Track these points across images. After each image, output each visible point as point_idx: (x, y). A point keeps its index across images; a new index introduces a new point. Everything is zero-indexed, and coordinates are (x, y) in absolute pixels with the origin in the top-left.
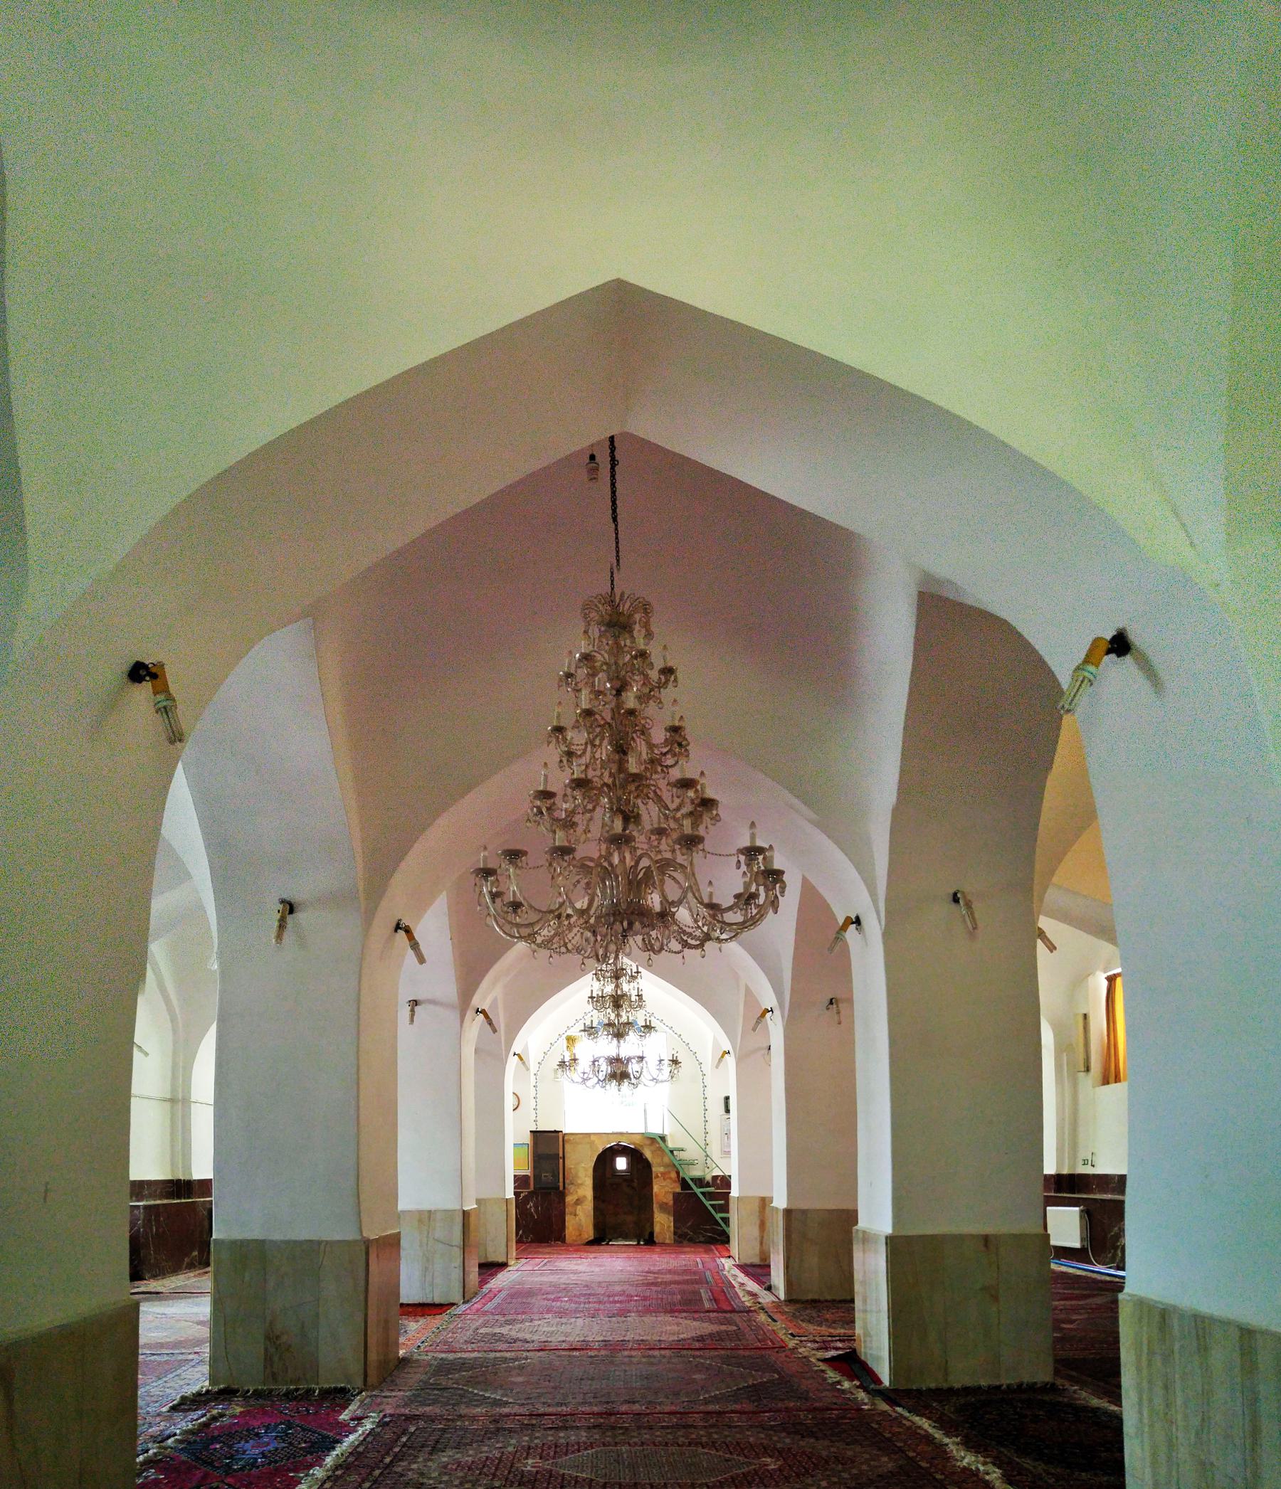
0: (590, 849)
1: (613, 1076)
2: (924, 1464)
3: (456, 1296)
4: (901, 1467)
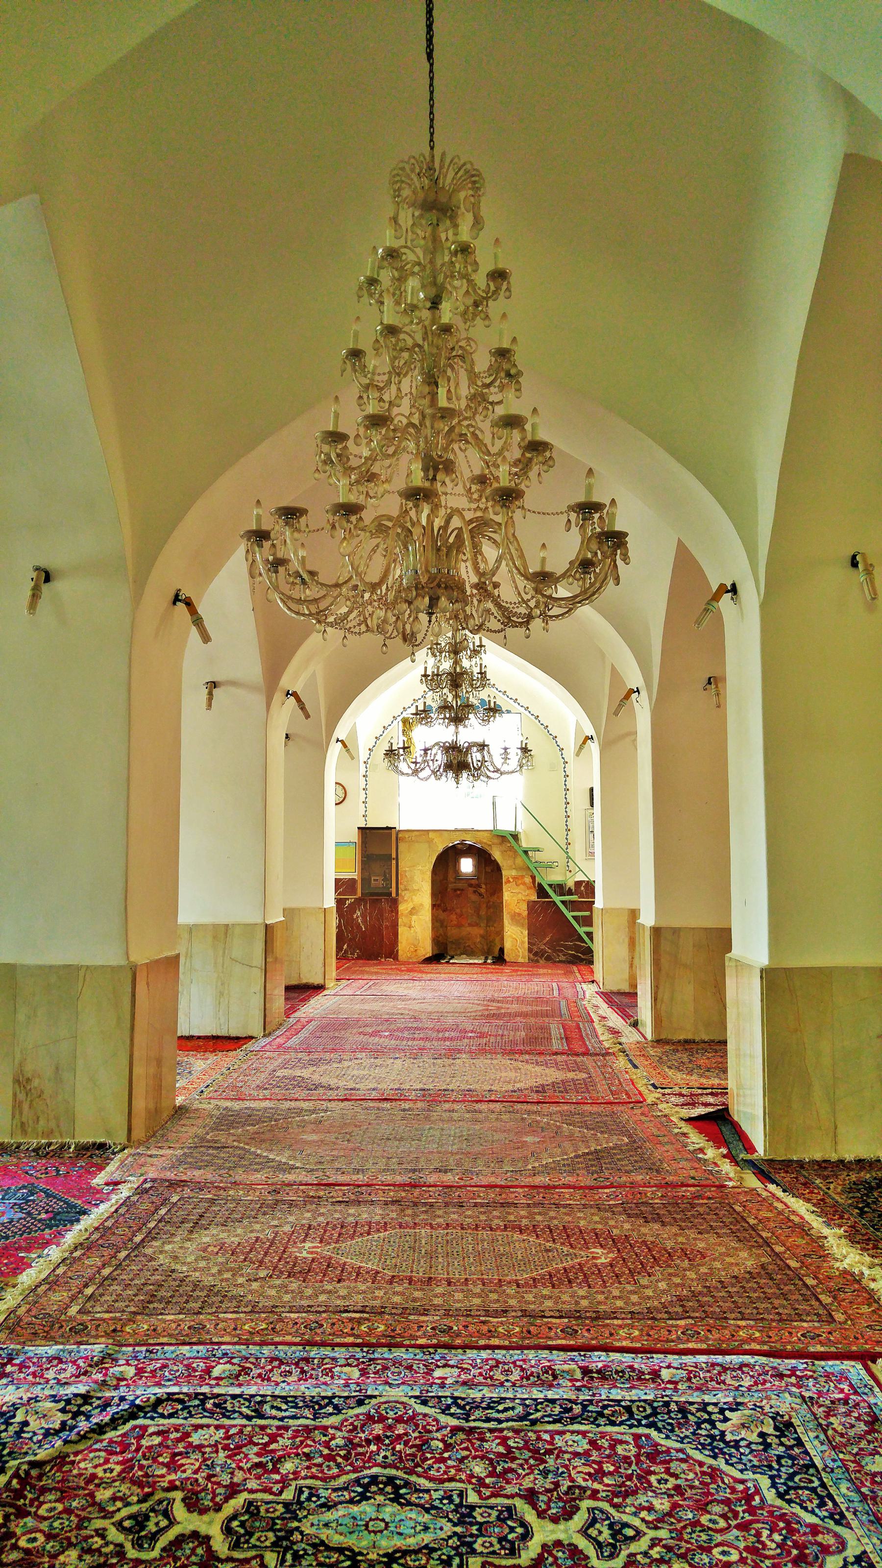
0: (385, 503)
1: (449, 766)
2: (793, 1264)
3: (256, 1029)
4: (763, 1266)
